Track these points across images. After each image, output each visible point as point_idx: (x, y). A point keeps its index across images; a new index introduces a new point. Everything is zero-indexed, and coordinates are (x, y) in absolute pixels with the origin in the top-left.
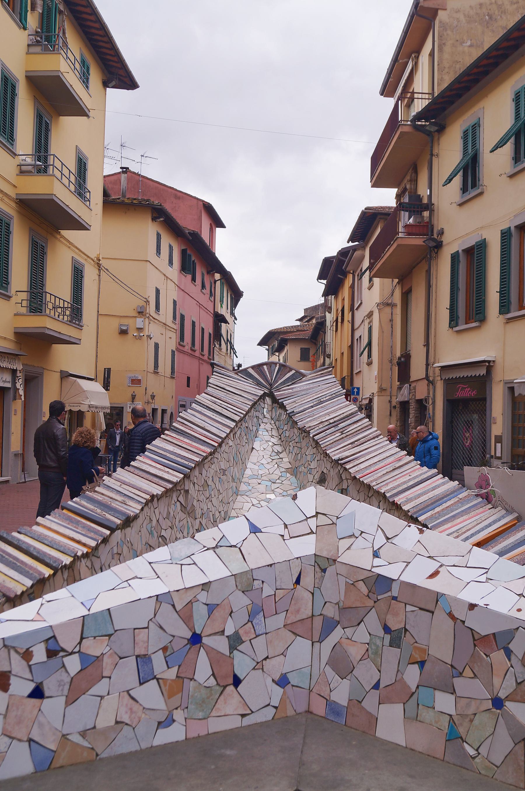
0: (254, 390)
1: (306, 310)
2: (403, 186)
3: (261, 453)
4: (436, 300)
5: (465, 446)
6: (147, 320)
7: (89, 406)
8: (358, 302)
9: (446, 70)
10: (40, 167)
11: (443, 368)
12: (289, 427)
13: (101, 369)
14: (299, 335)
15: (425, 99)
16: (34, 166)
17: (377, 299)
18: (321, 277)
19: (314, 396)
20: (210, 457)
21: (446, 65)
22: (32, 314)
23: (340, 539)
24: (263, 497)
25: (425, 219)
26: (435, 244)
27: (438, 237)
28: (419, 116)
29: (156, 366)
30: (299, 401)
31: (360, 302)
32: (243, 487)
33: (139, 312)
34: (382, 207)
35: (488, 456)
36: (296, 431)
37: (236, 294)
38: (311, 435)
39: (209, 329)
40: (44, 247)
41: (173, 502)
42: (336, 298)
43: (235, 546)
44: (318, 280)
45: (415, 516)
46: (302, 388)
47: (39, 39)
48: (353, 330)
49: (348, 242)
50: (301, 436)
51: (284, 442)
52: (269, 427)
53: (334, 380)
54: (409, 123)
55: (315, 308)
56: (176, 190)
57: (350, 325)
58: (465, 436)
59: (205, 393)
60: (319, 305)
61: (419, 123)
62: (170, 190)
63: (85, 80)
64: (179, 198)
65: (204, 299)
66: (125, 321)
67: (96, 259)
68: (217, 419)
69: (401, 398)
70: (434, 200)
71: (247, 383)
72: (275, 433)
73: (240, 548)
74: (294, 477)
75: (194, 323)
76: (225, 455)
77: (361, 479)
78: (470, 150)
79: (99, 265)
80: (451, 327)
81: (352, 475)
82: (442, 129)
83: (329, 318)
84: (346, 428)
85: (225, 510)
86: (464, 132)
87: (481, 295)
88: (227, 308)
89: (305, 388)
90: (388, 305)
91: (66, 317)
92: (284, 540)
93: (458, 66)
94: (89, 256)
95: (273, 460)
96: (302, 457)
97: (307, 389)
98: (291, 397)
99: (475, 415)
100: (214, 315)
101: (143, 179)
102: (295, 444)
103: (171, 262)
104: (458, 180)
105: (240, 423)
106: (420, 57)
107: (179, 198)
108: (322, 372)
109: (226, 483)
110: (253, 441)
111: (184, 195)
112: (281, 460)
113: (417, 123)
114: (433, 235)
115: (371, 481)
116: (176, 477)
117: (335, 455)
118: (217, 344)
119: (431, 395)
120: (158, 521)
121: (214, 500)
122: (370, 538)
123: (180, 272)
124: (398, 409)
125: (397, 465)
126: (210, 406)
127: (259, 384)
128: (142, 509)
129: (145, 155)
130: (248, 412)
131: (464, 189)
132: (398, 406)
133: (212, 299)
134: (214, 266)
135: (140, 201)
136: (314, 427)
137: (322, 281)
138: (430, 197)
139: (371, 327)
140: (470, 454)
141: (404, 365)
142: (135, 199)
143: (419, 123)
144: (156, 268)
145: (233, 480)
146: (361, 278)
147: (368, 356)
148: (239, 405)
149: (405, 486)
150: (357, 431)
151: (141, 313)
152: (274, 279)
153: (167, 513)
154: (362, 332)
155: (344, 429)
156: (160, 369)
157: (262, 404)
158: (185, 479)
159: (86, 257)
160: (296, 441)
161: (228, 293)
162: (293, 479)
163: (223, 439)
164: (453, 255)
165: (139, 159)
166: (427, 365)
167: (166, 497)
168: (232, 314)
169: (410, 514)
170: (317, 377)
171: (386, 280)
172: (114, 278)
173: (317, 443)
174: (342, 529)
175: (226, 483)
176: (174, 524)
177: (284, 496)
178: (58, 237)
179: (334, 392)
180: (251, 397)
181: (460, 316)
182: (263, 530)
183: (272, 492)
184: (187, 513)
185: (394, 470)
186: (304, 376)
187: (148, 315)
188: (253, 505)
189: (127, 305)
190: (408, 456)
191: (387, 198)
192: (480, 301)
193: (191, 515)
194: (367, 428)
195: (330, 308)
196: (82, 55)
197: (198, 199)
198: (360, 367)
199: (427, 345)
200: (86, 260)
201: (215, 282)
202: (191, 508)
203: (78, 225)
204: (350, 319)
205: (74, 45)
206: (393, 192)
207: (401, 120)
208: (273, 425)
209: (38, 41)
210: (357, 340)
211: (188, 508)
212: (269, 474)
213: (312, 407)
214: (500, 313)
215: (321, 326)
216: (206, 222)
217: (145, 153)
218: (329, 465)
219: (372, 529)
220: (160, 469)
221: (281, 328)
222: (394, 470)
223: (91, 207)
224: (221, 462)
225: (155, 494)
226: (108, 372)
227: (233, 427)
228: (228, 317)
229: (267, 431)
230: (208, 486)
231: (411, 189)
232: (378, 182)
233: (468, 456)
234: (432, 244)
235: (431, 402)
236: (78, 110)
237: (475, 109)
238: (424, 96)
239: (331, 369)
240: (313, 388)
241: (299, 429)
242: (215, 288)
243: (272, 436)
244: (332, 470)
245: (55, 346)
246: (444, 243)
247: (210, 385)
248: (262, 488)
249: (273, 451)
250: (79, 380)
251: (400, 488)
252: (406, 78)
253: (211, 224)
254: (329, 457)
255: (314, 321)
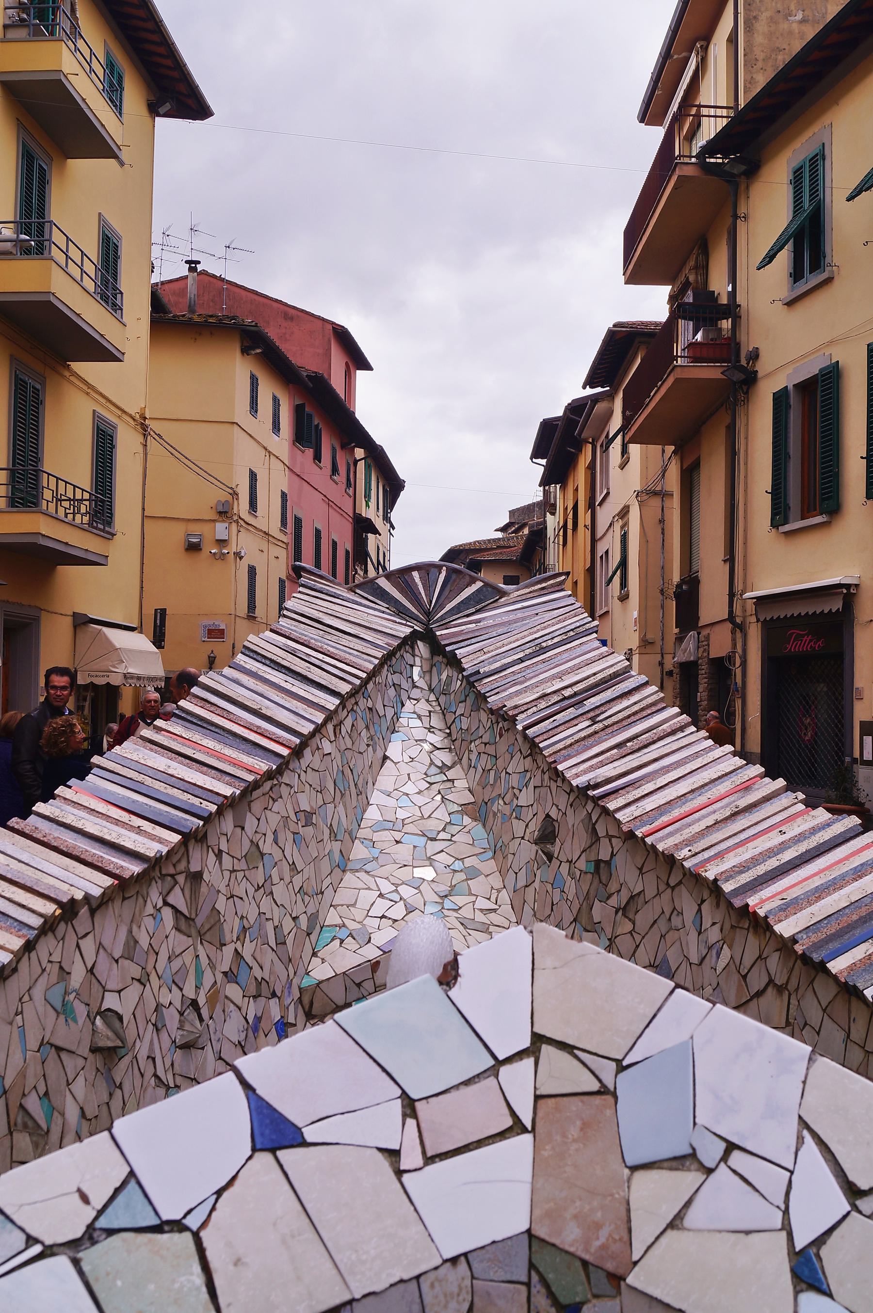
0: (390, 624)
1: (512, 513)
2: (682, 279)
3: (405, 769)
4: (746, 477)
5: (803, 741)
6: (234, 525)
7: (126, 676)
8: (601, 492)
9: (760, 64)
10: (27, 244)
11: (762, 601)
12: (469, 709)
13: (149, 612)
14: (501, 553)
15: (722, 117)
16: (16, 242)
17: (637, 485)
18: (536, 454)
19: (525, 637)
20: (268, 785)
21: (761, 56)
22: (15, 509)
23: (634, 1169)
24: (404, 874)
25: (723, 333)
26: (743, 377)
27: (748, 364)
28: (710, 148)
29: (252, 605)
30: (491, 648)
31: (605, 492)
32: (359, 851)
33: (220, 513)
34: (642, 323)
35: (848, 759)
36: (483, 716)
37: (393, 486)
38: (520, 727)
39: (346, 544)
40: (38, 390)
41: (149, 909)
42: (564, 488)
43: (178, 1226)
44: (531, 459)
45: (816, 957)
46: (498, 620)
47: (25, 16)
48: (594, 541)
49: (584, 387)
50: (497, 730)
51: (458, 743)
52: (423, 707)
53: (572, 600)
54: (694, 160)
55: (529, 509)
56: (286, 305)
57: (588, 533)
58: (803, 723)
59: (272, 631)
60: (534, 503)
61: (712, 160)
62: (275, 305)
63: (113, 93)
64: (292, 319)
65: (336, 491)
66: (196, 529)
67: (138, 416)
68: (294, 689)
69: (681, 657)
70: (740, 299)
71: (375, 609)
72: (436, 721)
73: (196, 1236)
74: (480, 826)
75: (318, 533)
76: (312, 777)
77: (649, 840)
78: (806, 204)
79: (144, 427)
80: (775, 525)
81: (625, 829)
82: (753, 169)
83: (552, 522)
84: (603, 709)
85: (311, 910)
86: (795, 173)
87: (831, 466)
88: (378, 508)
89: (505, 619)
90: (655, 493)
91: (78, 517)
92: (399, 1173)
93: (780, 57)
94: (126, 409)
95: (431, 784)
96: (498, 778)
97: (509, 623)
98: (473, 641)
99: (822, 685)
100: (353, 519)
101: (229, 286)
102: (482, 748)
103: (276, 427)
104: (784, 258)
105: (353, 701)
106: (712, 46)
107: (292, 319)
108: (544, 585)
109: (313, 845)
110: (386, 741)
111: (300, 314)
112: (449, 785)
113: (708, 160)
114: (739, 361)
115: (678, 847)
116: (154, 842)
117: (577, 775)
118: (361, 569)
119: (739, 649)
120: (91, 971)
121: (279, 891)
122: (771, 1180)
123: (294, 444)
124: (676, 677)
125: (743, 803)
126: (279, 660)
127: (400, 611)
128: (29, 947)
129: (233, 246)
130: (372, 675)
131: (797, 275)
132: (676, 671)
133: (351, 492)
134: (353, 434)
135: (221, 320)
136: (525, 707)
137: (539, 461)
138: (733, 295)
139: (625, 533)
140: (813, 756)
141: (687, 596)
142: (211, 316)
143: (712, 160)
144: (251, 436)
145: (334, 835)
146: (607, 448)
147: (621, 584)
148: (351, 658)
149: (773, 863)
150: (629, 716)
151: (224, 513)
152: (457, 465)
153: (127, 944)
154: (611, 544)
155: (597, 712)
156: (259, 612)
157: (408, 657)
158: (191, 845)
159: (120, 413)
160: (485, 740)
161: (378, 483)
162: (479, 830)
163: (306, 741)
164: (776, 396)
165: (221, 251)
166: (732, 595)
167: (124, 899)
168: (387, 518)
169: (799, 948)
170: (531, 595)
171: (651, 447)
172: (173, 450)
173: (533, 747)
174: (644, 1121)
175: (313, 845)
176: (150, 967)
177: (455, 871)
178: (67, 374)
179: (573, 627)
180: (381, 641)
181: (791, 505)
182: (310, 1134)
183: (427, 863)
184: (193, 932)
185: (734, 815)
186: (503, 594)
187: (235, 518)
188: (381, 895)
189: (201, 499)
190: (767, 780)
191: (652, 304)
192: (830, 476)
193: (207, 937)
194: (654, 709)
195: (554, 506)
196: (108, 54)
197: (323, 320)
198: (606, 605)
199: (730, 559)
200: (119, 417)
201: (356, 462)
202: (208, 918)
203: (102, 353)
204: (588, 522)
205: (94, 35)
206: (663, 291)
207: (680, 156)
208: (434, 704)
209: (22, 20)
210: (601, 557)
211: (199, 921)
212: (422, 817)
213: (521, 660)
214: (868, 497)
215: (538, 536)
216: (338, 361)
217: (231, 243)
218: (563, 801)
219: (778, 1139)
220: (117, 822)
221: (470, 544)
222: (734, 815)
223: (124, 320)
224: (300, 793)
225: (79, 896)
226: (161, 615)
227: (332, 708)
228: (379, 523)
229: (419, 717)
230: (262, 855)
231: (697, 281)
232: (638, 272)
233: (810, 760)
234: (738, 376)
235: (738, 662)
236: (99, 147)
237: (815, 128)
238: (719, 112)
239: (564, 577)
240: (523, 619)
241: (492, 712)
242: (355, 472)
243: (430, 729)
244: (570, 812)
245: (61, 568)
246: (760, 375)
247: (285, 612)
248: (403, 852)
249: (432, 763)
250: (105, 630)
251: (761, 870)
252: (685, 87)
253: (347, 363)
254: (564, 779)
255: (526, 531)
